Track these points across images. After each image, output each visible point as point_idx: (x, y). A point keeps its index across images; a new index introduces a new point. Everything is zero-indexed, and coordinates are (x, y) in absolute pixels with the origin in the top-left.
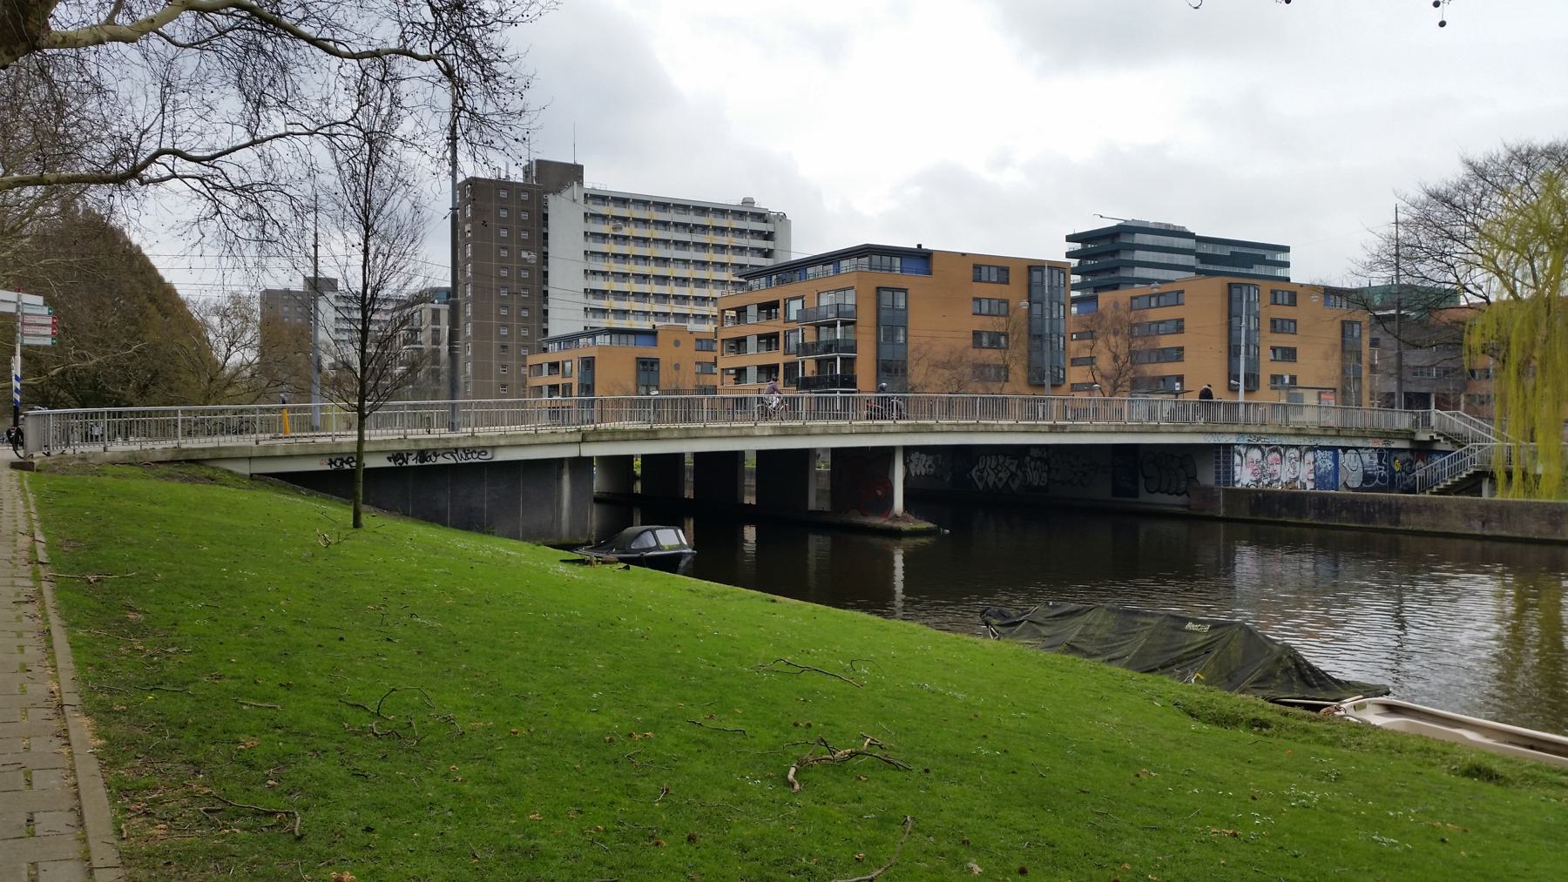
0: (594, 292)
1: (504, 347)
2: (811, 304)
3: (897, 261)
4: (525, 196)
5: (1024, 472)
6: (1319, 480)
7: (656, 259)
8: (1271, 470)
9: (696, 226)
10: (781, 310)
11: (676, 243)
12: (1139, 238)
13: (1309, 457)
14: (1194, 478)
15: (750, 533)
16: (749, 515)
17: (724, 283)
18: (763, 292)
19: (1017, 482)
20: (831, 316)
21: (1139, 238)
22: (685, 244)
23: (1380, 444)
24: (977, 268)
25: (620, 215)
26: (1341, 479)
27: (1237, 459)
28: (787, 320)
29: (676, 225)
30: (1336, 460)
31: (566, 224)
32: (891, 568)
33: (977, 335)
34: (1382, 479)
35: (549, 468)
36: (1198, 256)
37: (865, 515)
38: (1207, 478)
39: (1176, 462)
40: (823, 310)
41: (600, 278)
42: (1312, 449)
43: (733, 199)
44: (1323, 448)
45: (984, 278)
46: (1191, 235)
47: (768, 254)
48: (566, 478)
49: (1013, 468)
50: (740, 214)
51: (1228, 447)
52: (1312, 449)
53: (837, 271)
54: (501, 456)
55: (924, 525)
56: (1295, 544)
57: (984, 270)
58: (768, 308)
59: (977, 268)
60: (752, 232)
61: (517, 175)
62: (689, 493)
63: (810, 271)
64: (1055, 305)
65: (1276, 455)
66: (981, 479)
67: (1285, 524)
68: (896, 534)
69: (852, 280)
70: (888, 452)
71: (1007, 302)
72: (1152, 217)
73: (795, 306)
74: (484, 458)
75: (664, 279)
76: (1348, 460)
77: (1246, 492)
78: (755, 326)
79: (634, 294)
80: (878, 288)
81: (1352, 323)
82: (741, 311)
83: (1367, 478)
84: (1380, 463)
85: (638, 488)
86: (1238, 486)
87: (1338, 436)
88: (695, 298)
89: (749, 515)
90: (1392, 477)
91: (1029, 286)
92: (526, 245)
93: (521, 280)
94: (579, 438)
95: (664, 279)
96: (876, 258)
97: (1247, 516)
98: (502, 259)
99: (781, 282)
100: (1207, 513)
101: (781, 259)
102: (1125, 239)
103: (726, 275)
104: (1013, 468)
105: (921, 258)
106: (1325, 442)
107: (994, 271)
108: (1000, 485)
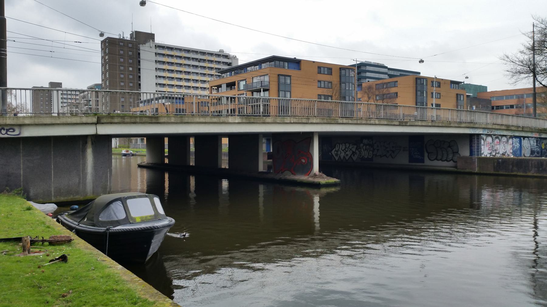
0: (160, 84)
1: (122, 106)
2: (249, 81)
3: (286, 64)
4: (130, 45)
5: (360, 152)
6: (514, 153)
7: (185, 72)
8: (495, 148)
9: (201, 59)
10: (236, 87)
11: (193, 66)
12: (368, 68)
13: (510, 141)
14: (457, 152)
15: (225, 184)
16: (224, 174)
17: (212, 75)
18: (228, 78)
19: (356, 156)
20: (259, 87)
21: (368, 68)
22: (197, 67)
23: (537, 135)
24: (319, 68)
25: (167, 52)
26: (523, 152)
27: (482, 141)
28: (239, 90)
29: (193, 59)
30: (520, 143)
31: (147, 55)
32: (312, 203)
33: (320, 96)
34: (538, 153)
35: (79, 141)
36: (389, 75)
37: (295, 174)
38: (465, 152)
39: (445, 144)
40: (255, 85)
41: (162, 79)
42: (511, 137)
43: (216, 50)
44: (516, 137)
45: (322, 72)
46: (386, 67)
47: (229, 64)
48: (89, 152)
49: (354, 150)
50: (218, 55)
51: (478, 135)
52: (511, 137)
53: (261, 68)
54: (27, 133)
55: (332, 180)
56: (505, 186)
57: (322, 69)
58: (231, 85)
59: (319, 68)
60: (223, 63)
61: (127, 37)
62: (192, 163)
63: (249, 69)
64: (351, 84)
65: (497, 140)
66: (337, 155)
67: (516, 176)
68: (317, 186)
69: (267, 71)
70: (309, 136)
71: (331, 82)
72: (373, 61)
73: (242, 83)
74: (12, 134)
75: (188, 80)
76: (525, 143)
77: (486, 159)
78: (224, 92)
79: (176, 86)
80: (279, 75)
81: (460, 95)
82: (219, 86)
83: (532, 152)
84: (537, 145)
85: (167, 161)
86: (483, 156)
87: (523, 131)
88: (201, 88)
89: (224, 174)
90: (541, 152)
91: (340, 76)
92: (130, 65)
93: (129, 79)
94: (95, 120)
95: (188, 80)
96: (277, 62)
97: (492, 172)
98: (121, 70)
99: (236, 74)
100: (467, 170)
101: (234, 65)
102: (363, 68)
103: (213, 72)
104: (354, 150)
105: (296, 63)
106: (517, 134)
107: (326, 69)
108: (347, 158)
